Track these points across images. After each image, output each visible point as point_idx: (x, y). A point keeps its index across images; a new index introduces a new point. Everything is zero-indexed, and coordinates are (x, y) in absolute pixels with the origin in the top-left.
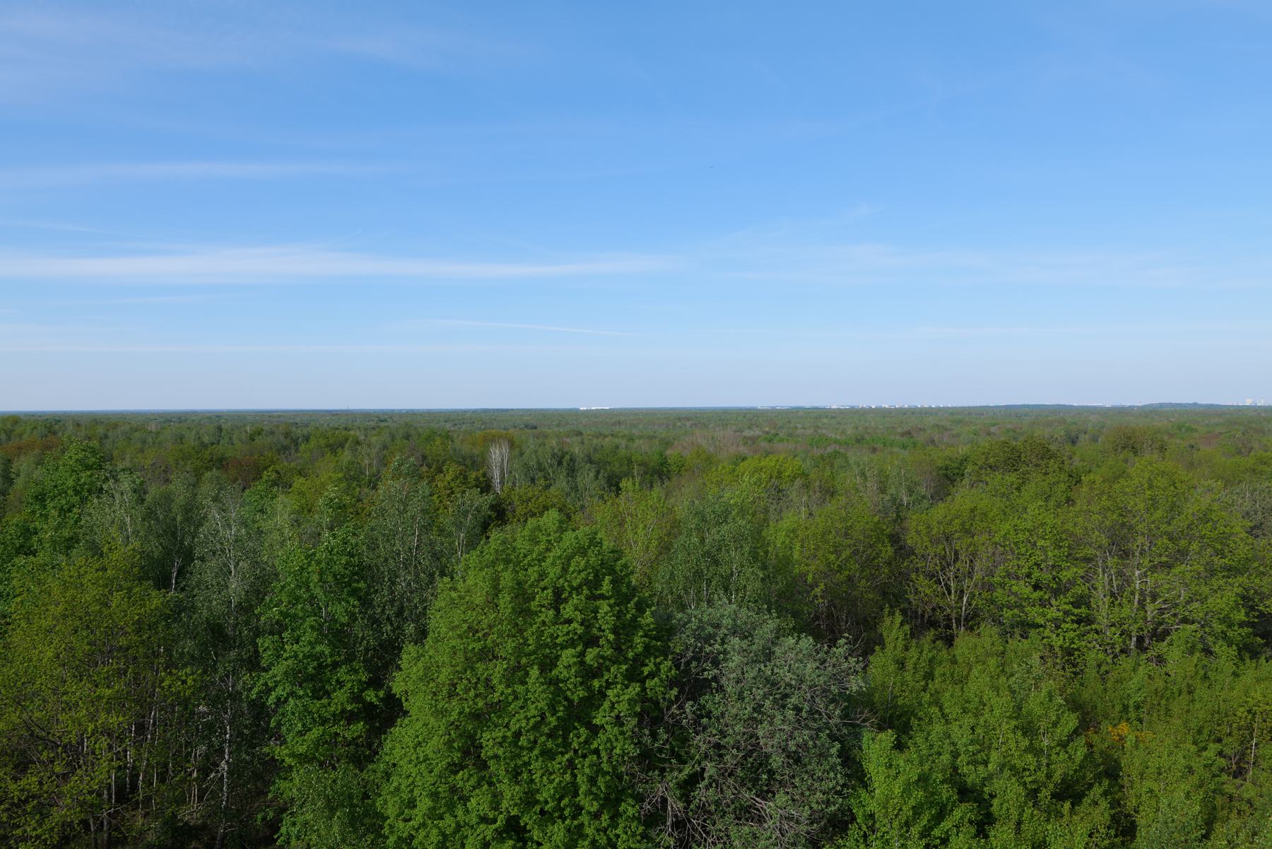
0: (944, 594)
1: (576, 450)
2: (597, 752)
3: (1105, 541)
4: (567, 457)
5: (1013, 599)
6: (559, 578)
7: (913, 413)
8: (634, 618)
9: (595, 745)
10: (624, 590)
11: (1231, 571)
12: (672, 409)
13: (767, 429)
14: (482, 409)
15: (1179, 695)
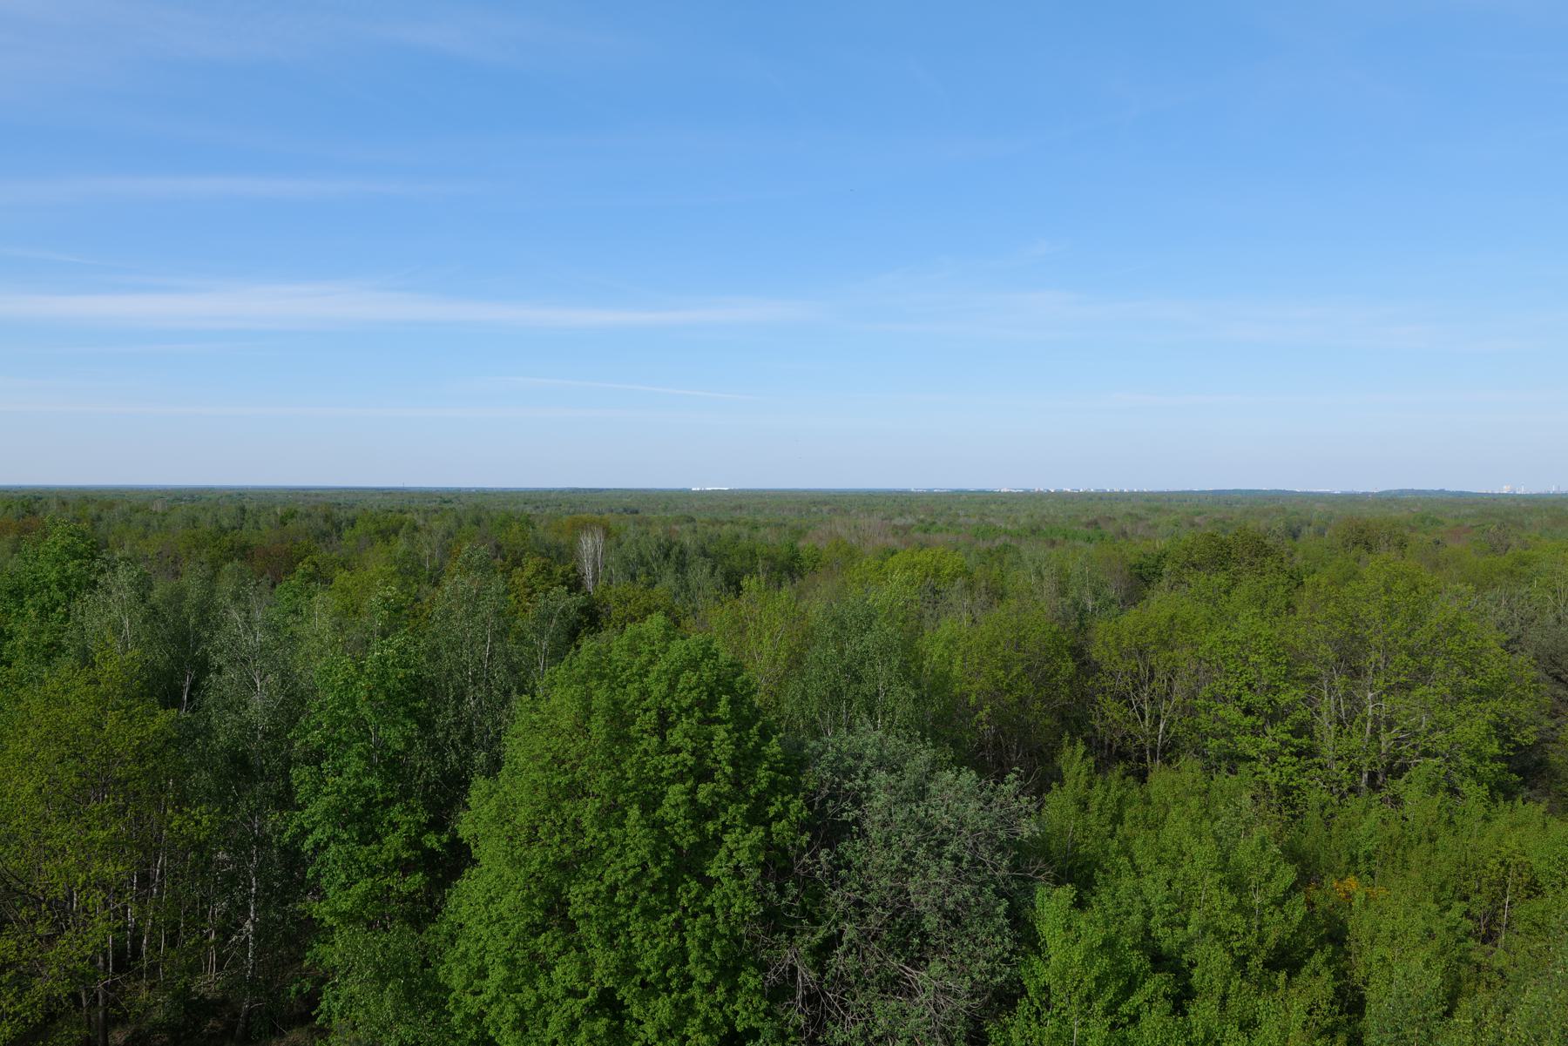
1: (687, 540)
2: (710, 910)
4: (676, 549)
5: (1219, 726)
6: (664, 698)
7: (1101, 498)
8: (757, 747)
9: (708, 902)
10: (745, 712)
11: (1482, 694)
12: (805, 491)
13: (922, 517)
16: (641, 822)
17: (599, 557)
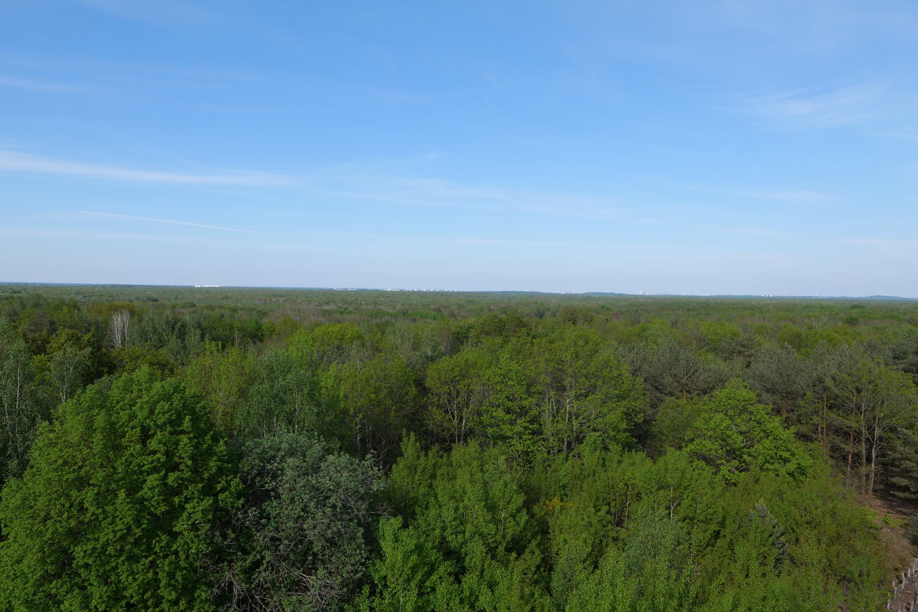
0: (450, 419)
1: (187, 318)
2: (176, 553)
3: (549, 380)
4: (179, 324)
5: (493, 421)
6: (145, 419)
7: (442, 295)
8: (210, 447)
9: (174, 547)
10: (202, 426)
11: (621, 398)
14: (110, 285)
15: (588, 477)
16: (127, 500)
17: (126, 329)
